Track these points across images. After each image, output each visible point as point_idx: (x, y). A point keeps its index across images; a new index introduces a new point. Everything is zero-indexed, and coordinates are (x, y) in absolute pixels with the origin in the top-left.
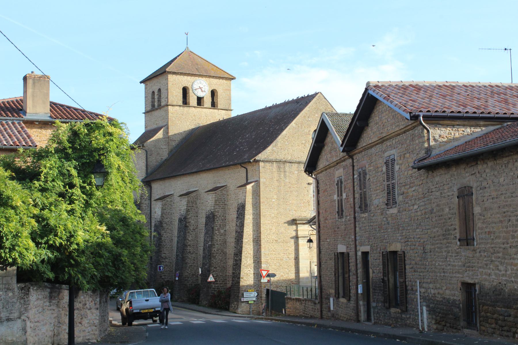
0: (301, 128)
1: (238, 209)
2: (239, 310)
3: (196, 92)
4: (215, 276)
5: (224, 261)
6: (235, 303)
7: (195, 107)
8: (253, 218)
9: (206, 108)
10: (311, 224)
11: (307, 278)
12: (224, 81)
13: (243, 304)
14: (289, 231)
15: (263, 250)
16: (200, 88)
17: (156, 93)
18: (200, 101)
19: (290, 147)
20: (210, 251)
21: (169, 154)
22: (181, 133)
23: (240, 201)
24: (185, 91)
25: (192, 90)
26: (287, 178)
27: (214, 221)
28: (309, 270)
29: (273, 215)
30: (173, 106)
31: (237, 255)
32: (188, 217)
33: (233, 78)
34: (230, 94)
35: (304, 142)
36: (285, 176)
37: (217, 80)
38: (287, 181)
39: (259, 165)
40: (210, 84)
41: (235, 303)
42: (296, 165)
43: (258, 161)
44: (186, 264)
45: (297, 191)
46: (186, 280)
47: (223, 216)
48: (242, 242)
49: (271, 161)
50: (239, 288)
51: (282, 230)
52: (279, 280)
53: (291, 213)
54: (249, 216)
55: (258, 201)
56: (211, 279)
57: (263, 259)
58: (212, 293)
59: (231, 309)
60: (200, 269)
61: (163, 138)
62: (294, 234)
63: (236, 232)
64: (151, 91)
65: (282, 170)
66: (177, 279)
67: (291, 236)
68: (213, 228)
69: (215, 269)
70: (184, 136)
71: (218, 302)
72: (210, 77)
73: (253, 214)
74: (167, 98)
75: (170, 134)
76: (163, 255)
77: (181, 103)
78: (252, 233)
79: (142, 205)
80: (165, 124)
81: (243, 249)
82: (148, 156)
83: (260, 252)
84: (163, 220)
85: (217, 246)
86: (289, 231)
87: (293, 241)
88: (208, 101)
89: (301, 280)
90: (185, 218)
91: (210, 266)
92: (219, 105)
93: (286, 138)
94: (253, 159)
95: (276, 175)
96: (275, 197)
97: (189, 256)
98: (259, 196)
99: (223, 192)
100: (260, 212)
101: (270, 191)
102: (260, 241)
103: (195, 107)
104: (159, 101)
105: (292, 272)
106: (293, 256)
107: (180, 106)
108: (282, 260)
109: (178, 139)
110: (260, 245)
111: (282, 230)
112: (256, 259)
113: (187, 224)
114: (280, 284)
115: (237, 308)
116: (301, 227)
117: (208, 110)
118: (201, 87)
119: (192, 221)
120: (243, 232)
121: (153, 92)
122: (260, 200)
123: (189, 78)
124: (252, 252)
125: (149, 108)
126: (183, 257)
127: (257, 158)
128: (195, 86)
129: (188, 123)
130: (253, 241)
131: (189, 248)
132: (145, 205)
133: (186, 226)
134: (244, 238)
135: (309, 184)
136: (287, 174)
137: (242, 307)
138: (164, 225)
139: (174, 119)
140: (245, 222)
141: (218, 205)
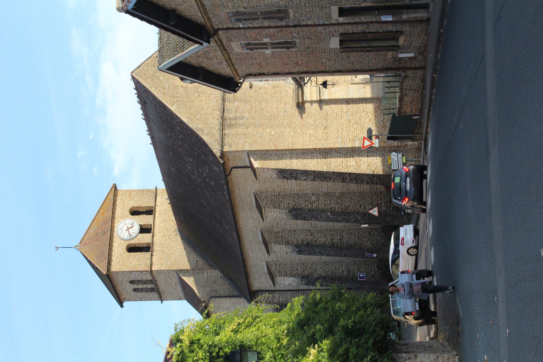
1: (284, 178)
3: (134, 235)
4: (370, 207)
5: (352, 195)
7: (153, 236)
8: (296, 159)
11: (373, 88)
15: (338, 146)
16: (128, 229)
18: (144, 230)
19: (204, 112)
20: (339, 214)
21: (215, 269)
22: (187, 253)
24: (132, 249)
25: (131, 239)
26: (243, 115)
27: (300, 209)
28: (362, 86)
30: (151, 265)
31: (343, 178)
32: (295, 242)
35: (196, 94)
36: (242, 118)
37: (117, 207)
38: (247, 115)
40: (123, 217)
42: (226, 103)
43: (222, 153)
44: (356, 244)
46: (377, 244)
47: (294, 198)
48: (327, 172)
50: (386, 175)
51: (311, 121)
53: (290, 109)
54: (294, 165)
56: (375, 212)
57: (349, 145)
60: (363, 226)
62: (316, 105)
63: (314, 180)
64: (133, 293)
65: (233, 122)
66: (375, 255)
67: (319, 109)
69: (363, 207)
70: (190, 250)
72: (113, 217)
73: (291, 158)
75: (188, 267)
76: (345, 274)
77: (147, 255)
78: (315, 160)
80: (175, 274)
81: (335, 170)
82: (218, 295)
83: (339, 149)
84: (299, 275)
85: (332, 204)
87: (325, 107)
88: (145, 220)
89: (375, 96)
90: (297, 246)
91: (358, 213)
92: (150, 205)
94: (220, 160)
95: (240, 130)
96: (268, 130)
97: (345, 240)
98: (268, 151)
100: (289, 150)
101: (261, 137)
102: (325, 149)
103: (153, 236)
104: (146, 282)
105: (365, 107)
106: (344, 107)
107: (152, 255)
108: (349, 121)
109: (194, 256)
110: (331, 149)
111: (311, 121)
112: (349, 155)
113: (305, 243)
114: (381, 122)
116: (308, 96)
117: (156, 219)
118: (127, 228)
120: (314, 172)
121: (135, 290)
123: (115, 244)
125: (155, 295)
126: (347, 248)
127: (218, 154)
128: (126, 236)
129: (174, 244)
130: (325, 158)
131: (336, 241)
132: (281, 298)
133: (308, 245)
135: (251, 87)
136: (238, 115)
138: (306, 273)
139: (169, 263)
140: (301, 168)
141: (279, 204)
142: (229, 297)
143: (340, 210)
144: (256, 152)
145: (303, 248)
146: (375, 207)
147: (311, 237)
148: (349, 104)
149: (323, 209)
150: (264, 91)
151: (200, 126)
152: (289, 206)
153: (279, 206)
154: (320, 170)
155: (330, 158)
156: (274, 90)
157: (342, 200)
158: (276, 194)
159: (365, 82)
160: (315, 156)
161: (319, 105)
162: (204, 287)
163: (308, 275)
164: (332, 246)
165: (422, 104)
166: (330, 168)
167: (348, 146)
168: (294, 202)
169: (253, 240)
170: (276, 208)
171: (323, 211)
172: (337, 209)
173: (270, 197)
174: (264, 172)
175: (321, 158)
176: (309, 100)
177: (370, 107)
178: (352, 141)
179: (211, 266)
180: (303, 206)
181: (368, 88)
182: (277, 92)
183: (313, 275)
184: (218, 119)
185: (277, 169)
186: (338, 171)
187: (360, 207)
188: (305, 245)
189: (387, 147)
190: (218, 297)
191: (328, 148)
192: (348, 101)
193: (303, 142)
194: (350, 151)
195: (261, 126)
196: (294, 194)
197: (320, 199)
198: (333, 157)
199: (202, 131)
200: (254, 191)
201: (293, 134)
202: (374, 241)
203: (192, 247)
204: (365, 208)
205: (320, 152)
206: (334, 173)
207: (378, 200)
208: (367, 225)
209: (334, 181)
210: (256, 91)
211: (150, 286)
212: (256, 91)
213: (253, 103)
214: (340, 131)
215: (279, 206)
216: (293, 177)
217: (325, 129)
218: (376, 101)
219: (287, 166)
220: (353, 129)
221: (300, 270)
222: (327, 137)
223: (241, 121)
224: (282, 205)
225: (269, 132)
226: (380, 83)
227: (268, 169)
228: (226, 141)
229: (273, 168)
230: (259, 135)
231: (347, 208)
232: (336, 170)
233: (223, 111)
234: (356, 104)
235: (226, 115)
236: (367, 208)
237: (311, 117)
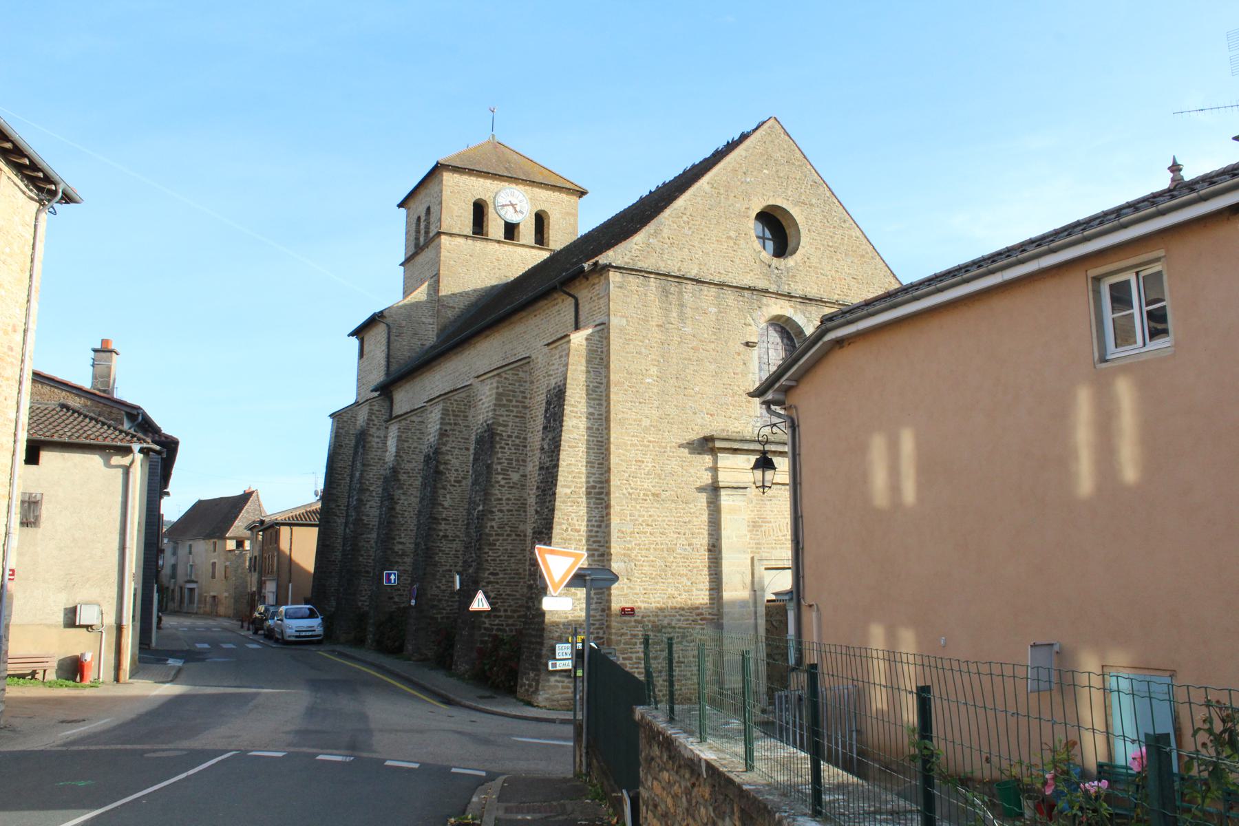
0: (727, 198)
1: (549, 403)
2: (541, 698)
3: (502, 213)
4: (492, 595)
5: (520, 557)
6: (532, 675)
7: (499, 242)
8: (588, 428)
11: (743, 604)
12: (564, 197)
13: (553, 679)
14: (692, 471)
15: (615, 521)
16: (512, 205)
17: (423, 219)
18: (511, 230)
19: (696, 244)
20: (480, 528)
21: (438, 336)
22: (467, 293)
23: (553, 382)
24: (479, 210)
26: (689, 322)
27: (492, 447)
28: (748, 580)
30: (451, 235)
31: (541, 533)
32: (444, 449)
33: (582, 193)
34: (576, 223)
35: (733, 234)
36: (682, 317)
37: (549, 193)
38: (688, 330)
39: (607, 279)
40: (533, 200)
41: (532, 675)
42: (713, 290)
43: (607, 267)
44: (435, 565)
46: (433, 607)
47: (517, 437)
48: (554, 494)
51: (673, 465)
52: (661, 609)
54: (575, 421)
55: (604, 381)
56: (480, 603)
57: (616, 548)
58: (482, 642)
59: (521, 691)
60: (458, 577)
61: (427, 302)
62: (707, 479)
63: (541, 468)
64: (416, 217)
65: (673, 299)
66: (413, 602)
67: (698, 484)
68: (489, 467)
69: (492, 578)
70: (473, 299)
71: (491, 668)
72: (533, 183)
73: (590, 416)
75: (442, 293)
76: (398, 548)
77: (468, 230)
78: (584, 470)
81: (557, 514)
83: (608, 526)
85: (501, 515)
87: (703, 498)
88: (527, 232)
89: (726, 610)
90: (437, 452)
91: (480, 568)
92: (551, 243)
93: (685, 218)
94: (590, 262)
95: (655, 309)
97: (445, 545)
98: (607, 367)
99: (521, 374)
100: (608, 412)
101: (640, 353)
102: (608, 494)
103: (499, 242)
105: (701, 586)
106: (703, 540)
107: (466, 237)
108: (671, 550)
109: (461, 305)
110: (608, 506)
111: (673, 465)
112: (595, 546)
113: (441, 468)
114: (666, 622)
115: (536, 691)
116: (725, 461)
118: (514, 203)
120: (557, 466)
121: (419, 218)
122: (608, 377)
124: (583, 527)
125: (412, 250)
127: (603, 259)
128: (502, 200)
129: (484, 274)
130: (588, 493)
131: (443, 526)
133: (438, 473)
135: (747, 344)
136: (689, 312)
138: (403, 477)
140: (565, 436)
142: (388, 357)
144: (605, 343)
146: (490, 604)
148: (709, 550)
150: (739, 370)
151: (665, 230)
152: (500, 425)
155: (588, 503)
156: (741, 392)
158: (527, 401)
159: (756, 587)
160: (594, 471)
162: (409, 316)
164: (434, 520)
165: (741, 441)
166: (564, 502)
168: (509, 436)
170: (497, 399)
175: (588, 482)
176: (720, 464)
177: (701, 597)
178: (624, 555)
179: (442, 330)
180: (500, 455)
181: (744, 594)
182: (737, 398)
184: (679, 270)
185: (565, 384)
187: (491, 574)
189: (610, 634)
190: (389, 338)
192: (715, 549)
193: (625, 444)
194: (602, 549)
195: (663, 357)
197: (514, 491)
198: (590, 509)
199: (656, 234)
202: (440, 601)
204: (489, 583)
205: (601, 482)
206: (552, 510)
207: (506, 611)
209: (537, 512)
211: (422, 239)
213: (713, 346)
214: (649, 529)
217: (653, 494)
218: (715, 611)
220: (652, 558)
222: (636, 500)
223: (675, 315)
224: (502, 411)
226: (752, 621)
227: (567, 365)
229: (569, 375)
233: (698, 281)
235: (690, 286)
236: (490, 587)
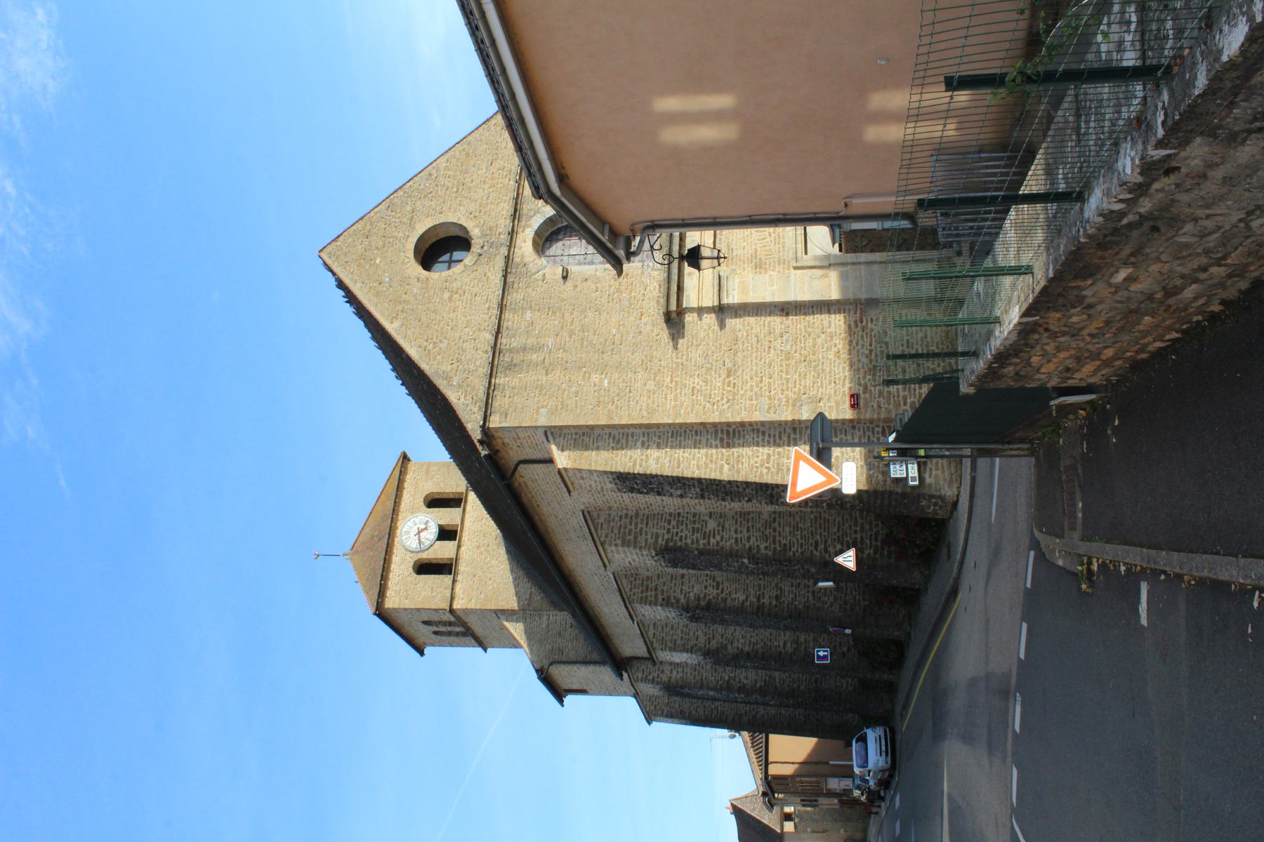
1: (632, 490)
2: (949, 492)
3: (427, 543)
4: (839, 546)
5: (797, 518)
6: (924, 503)
8: (659, 447)
9: (463, 521)
10: (621, 253)
11: (843, 278)
12: (409, 478)
13: (928, 480)
14: (702, 334)
15: (758, 417)
16: (419, 533)
17: (436, 629)
18: (447, 534)
19: (457, 335)
21: (561, 610)
22: (515, 579)
23: (609, 486)
24: (425, 568)
26: (542, 341)
27: (681, 549)
28: (819, 272)
29: (651, 385)
31: (771, 496)
32: (683, 601)
33: (405, 458)
34: (437, 464)
35: (446, 295)
36: (537, 348)
39: (497, 429)
40: (413, 511)
41: (924, 503)
42: (507, 315)
43: (485, 430)
44: (808, 608)
45: (583, 312)
47: (669, 522)
48: (729, 482)
49: (490, 390)
50: (875, 492)
51: (696, 355)
53: (649, 328)
54: (652, 462)
55: (607, 431)
56: (848, 560)
57: (786, 415)
59: (941, 514)
60: (821, 584)
62: (710, 319)
63: (703, 497)
64: (434, 636)
65: (517, 358)
66: (848, 631)
67: (716, 328)
68: (701, 553)
69: (821, 547)
70: (521, 573)
74: (436, 610)
76: (789, 649)
77: (447, 579)
78: (703, 451)
79: (673, 680)
83: (763, 423)
84: (700, 649)
85: (753, 539)
86: (702, 334)
87: (731, 323)
88: (448, 516)
89: (851, 296)
90: (686, 609)
92: (459, 490)
94: (480, 448)
95: (530, 377)
96: (595, 378)
97: (787, 599)
98: (592, 428)
99: (601, 520)
100: (640, 426)
101: (577, 393)
102: (728, 424)
103: (459, 547)
104: (445, 624)
105: (826, 323)
106: (776, 322)
107: (454, 581)
108: (788, 356)
109: (527, 585)
110: (742, 424)
111: (696, 355)
112: (785, 438)
113: (703, 603)
114: (865, 360)
118: (417, 531)
119: (696, 590)
120: (699, 480)
121: (436, 633)
122: (603, 427)
123: (396, 559)
124: (764, 451)
125: (469, 639)
126: (790, 616)
127: (476, 435)
128: (413, 544)
129: (494, 562)
130: (728, 446)
131: (766, 601)
132: (674, 673)
133: (708, 607)
134: (718, 477)
135: (565, 278)
136: (531, 341)
137: (937, 483)
138: (714, 644)
140: (668, 472)
141: (635, 537)
142: (585, 662)
143: (770, 554)
144: (567, 431)
145: (699, 611)
146: (848, 548)
147: (716, 591)
148: (787, 314)
149: (731, 550)
150: (593, 287)
151: (444, 368)
153: (635, 542)
154: (712, 477)
155: (739, 445)
157: (775, 530)
158: (630, 513)
160: (704, 441)
161: (717, 318)
163: (717, 649)
164: (759, 610)
167: (783, 419)
168: (668, 531)
169: (602, 588)
170: (629, 546)
171: (731, 556)
172: (763, 551)
173: (617, 519)
174: (582, 478)
175: (716, 447)
176: (695, 305)
177: (837, 323)
178: (794, 406)
179: (555, 605)
180: (689, 541)
182: (623, 288)
183: (726, 648)
184: (486, 352)
185: (612, 473)
186: (757, 480)
188: (702, 609)
189: (879, 420)
190: (565, 663)
191: (735, 423)
192: (786, 309)
194: (788, 430)
195: (580, 368)
196: (670, 515)
197: (727, 526)
199: (448, 378)
200: (582, 507)
201: (652, 388)
203: (524, 569)
204: (826, 551)
205: (716, 432)
206: (747, 484)
207: (855, 532)
208: (831, 584)
210: (576, 286)
212: (576, 286)
213: (567, 315)
214: (766, 380)
215: (635, 542)
216: (652, 489)
217: (728, 376)
219: (634, 465)
220: (796, 376)
221: (702, 639)
222: (734, 394)
223: (535, 356)
224: (641, 539)
225: (597, 381)
226: (862, 267)
227: (590, 471)
228: (496, 404)
230: (573, 389)
231: (785, 550)
232: (753, 478)
234: (805, 314)
235: (504, 340)
236: (831, 550)
237: (698, 346)
